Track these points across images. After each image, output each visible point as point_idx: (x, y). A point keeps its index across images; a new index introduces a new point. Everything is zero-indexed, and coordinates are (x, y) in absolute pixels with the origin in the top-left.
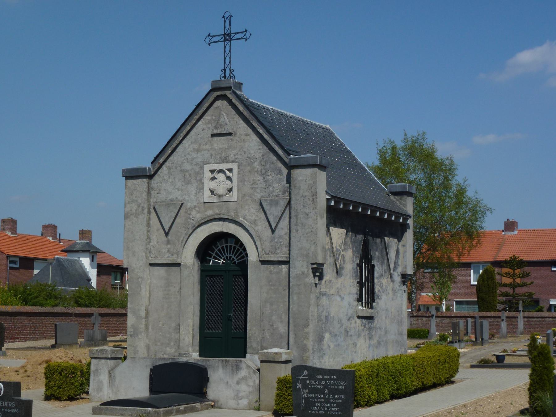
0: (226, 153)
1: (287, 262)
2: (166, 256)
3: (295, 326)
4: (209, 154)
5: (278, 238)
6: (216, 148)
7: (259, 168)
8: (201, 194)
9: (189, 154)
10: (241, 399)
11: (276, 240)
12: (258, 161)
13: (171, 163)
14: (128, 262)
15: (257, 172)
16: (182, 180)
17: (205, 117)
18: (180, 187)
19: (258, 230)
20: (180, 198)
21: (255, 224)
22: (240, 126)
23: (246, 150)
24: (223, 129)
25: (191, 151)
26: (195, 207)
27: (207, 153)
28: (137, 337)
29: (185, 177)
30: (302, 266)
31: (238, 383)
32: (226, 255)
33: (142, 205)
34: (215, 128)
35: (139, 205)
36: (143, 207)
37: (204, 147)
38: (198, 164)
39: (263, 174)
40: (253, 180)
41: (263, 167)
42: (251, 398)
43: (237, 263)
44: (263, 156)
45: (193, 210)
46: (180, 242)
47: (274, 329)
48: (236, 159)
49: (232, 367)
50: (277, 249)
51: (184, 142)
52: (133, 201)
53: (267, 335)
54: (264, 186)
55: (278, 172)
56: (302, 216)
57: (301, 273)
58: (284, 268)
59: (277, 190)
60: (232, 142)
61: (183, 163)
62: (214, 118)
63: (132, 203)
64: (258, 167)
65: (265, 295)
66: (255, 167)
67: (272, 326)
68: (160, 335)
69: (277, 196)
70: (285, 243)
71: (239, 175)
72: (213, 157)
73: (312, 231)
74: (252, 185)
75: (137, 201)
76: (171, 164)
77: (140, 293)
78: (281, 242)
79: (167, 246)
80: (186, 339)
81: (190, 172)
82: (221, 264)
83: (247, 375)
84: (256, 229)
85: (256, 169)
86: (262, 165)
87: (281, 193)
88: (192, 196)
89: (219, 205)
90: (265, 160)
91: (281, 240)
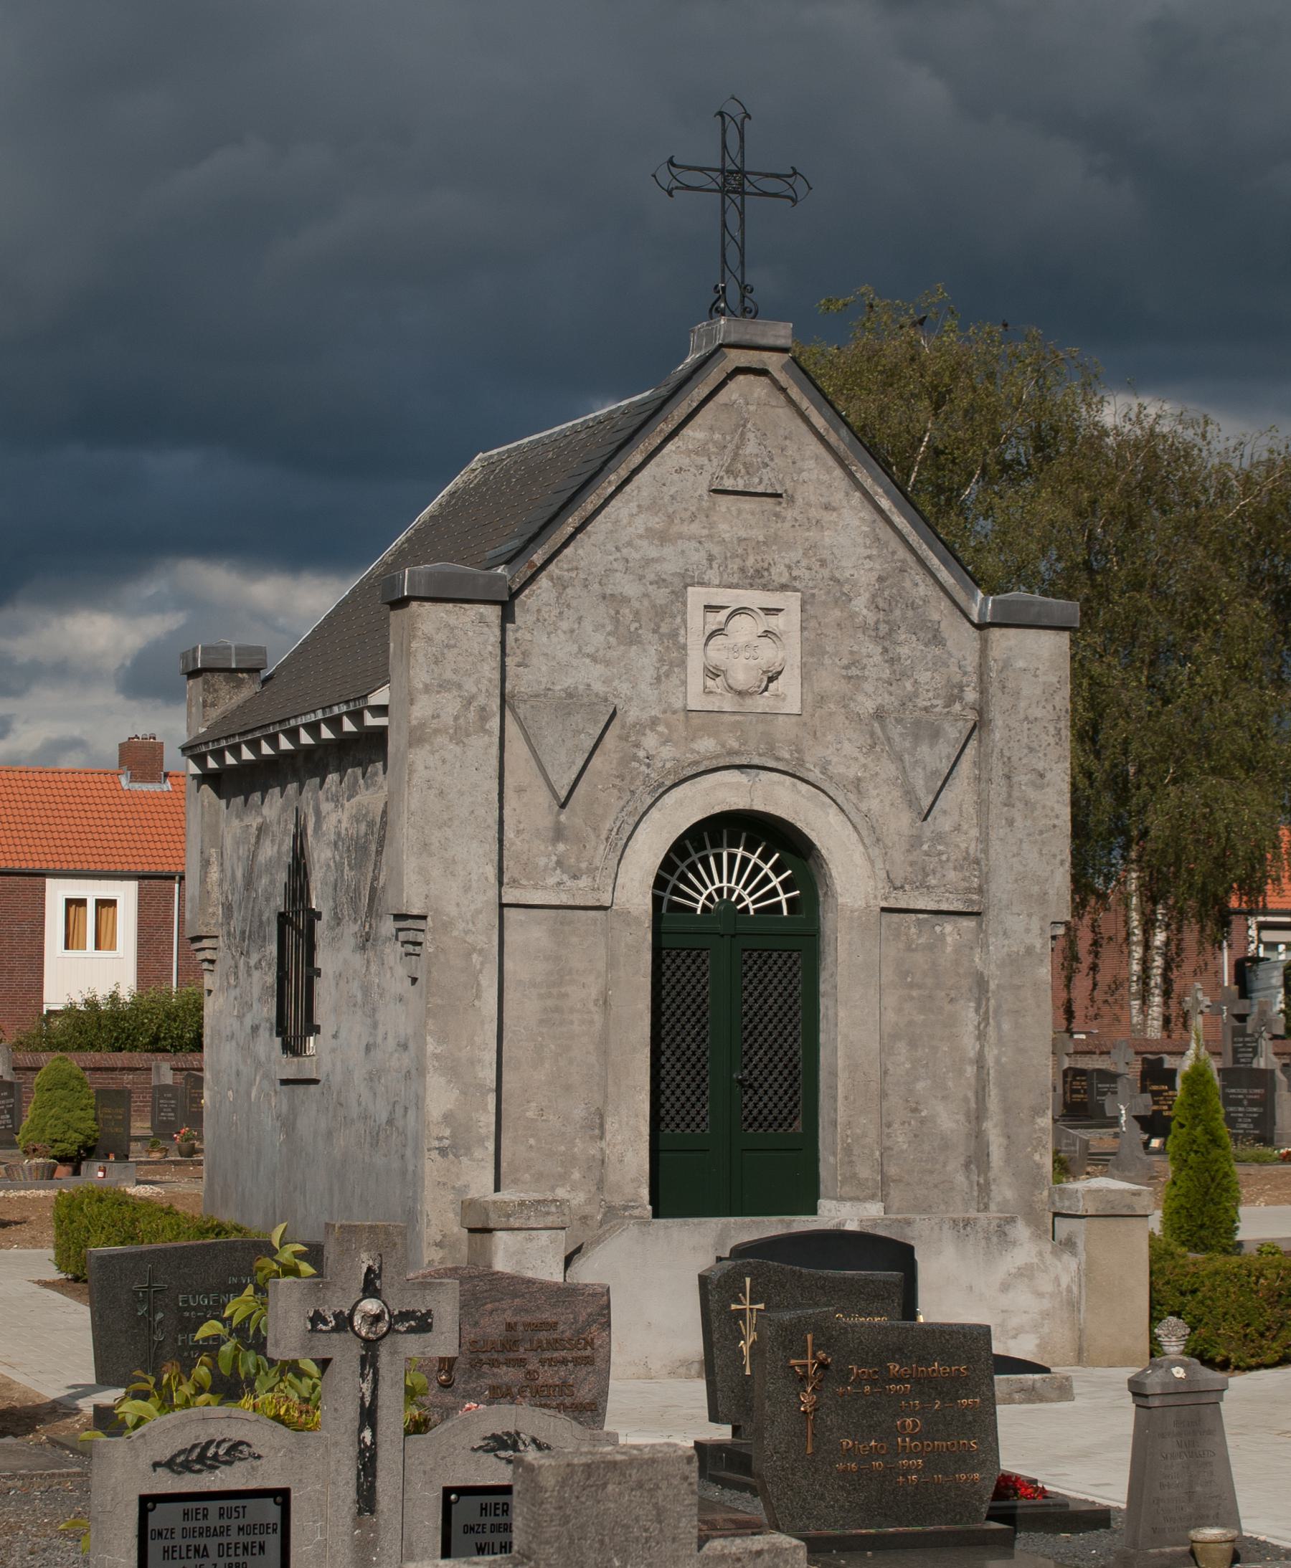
0: (759, 558)
1: (502, 906)
2: (551, 881)
3: (1006, 1110)
4: (703, 554)
5: (932, 840)
6: (727, 536)
7: (871, 617)
8: (674, 680)
9: (629, 544)
10: (1015, 1337)
11: (925, 847)
12: (867, 595)
13: (565, 566)
14: (427, 896)
15: (864, 627)
16: (609, 628)
17: (687, 431)
18: (601, 653)
19: (869, 810)
20: (598, 687)
21: (859, 792)
22: (805, 475)
23: (826, 554)
24: (756, 480)
25: (641, 537)
26: (654, 722)
27: (697, 550)
28: (466, 1155)
29: (616, 621)
30: (1028, 931)
31: (1005, 1287)
32: (732, 885)
33: (482, 700)
34: (727, 472)
35: (470, 701)
36: (483, 709)
37: (685, 529)
38: (664, 580)
39: (885, 636)
40: (852, 653)
41: (881, 615)
42: (1046, 1330)
43: (752, 913)
44: (881, 579)
45: (648, 731)
46: (603, 836)
47: (923, 1122)
48: (795, 578)
49: (988, 1239)
50: (928, 875)
51: (613, 502)
52: (444, 686)
53: (901, 1140)
54: (886, 674)
55: (930, 636)
56: (1024, 779)
57: (1022, 950)
58: (950, 934)
59: (928, 691)
60: (779, 525)
61: (609, 571)
62: (717, 436)
63: (438, 692)
64: (865, 611)
65: (891, 1016)
66: (856, 614)
67: (915, 1110)
68: (531, 1146)
69: (926, 709)
70: (953, 858)
71: (806, 633)
72: (715, 565)
73: (1054, 826)
74: (847, 667)
75: (459, 686)
76: (568, 570)
77: (476, 1003)
78: (940, 854)
79: (554, 845)
80: (629, 1157)
81: (636, 605)
82: (699, 912)
83: (1035, 1260)
84: (864, 806)
85: (859, 620)
86: (877, 607)
87: (939, 702)
88: (644, 687)
89: (738, 722)
90: (886, 593)
91: (940, 848)
